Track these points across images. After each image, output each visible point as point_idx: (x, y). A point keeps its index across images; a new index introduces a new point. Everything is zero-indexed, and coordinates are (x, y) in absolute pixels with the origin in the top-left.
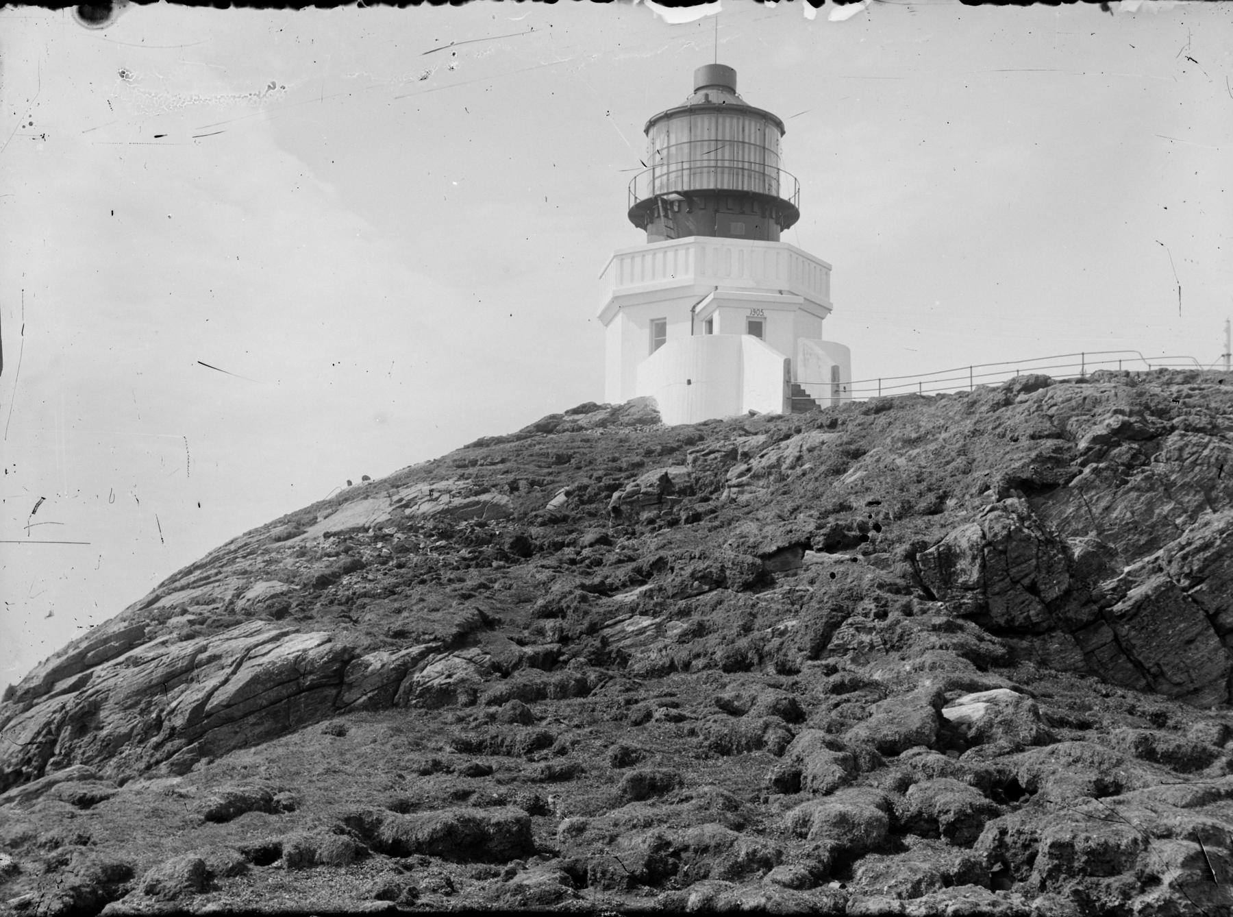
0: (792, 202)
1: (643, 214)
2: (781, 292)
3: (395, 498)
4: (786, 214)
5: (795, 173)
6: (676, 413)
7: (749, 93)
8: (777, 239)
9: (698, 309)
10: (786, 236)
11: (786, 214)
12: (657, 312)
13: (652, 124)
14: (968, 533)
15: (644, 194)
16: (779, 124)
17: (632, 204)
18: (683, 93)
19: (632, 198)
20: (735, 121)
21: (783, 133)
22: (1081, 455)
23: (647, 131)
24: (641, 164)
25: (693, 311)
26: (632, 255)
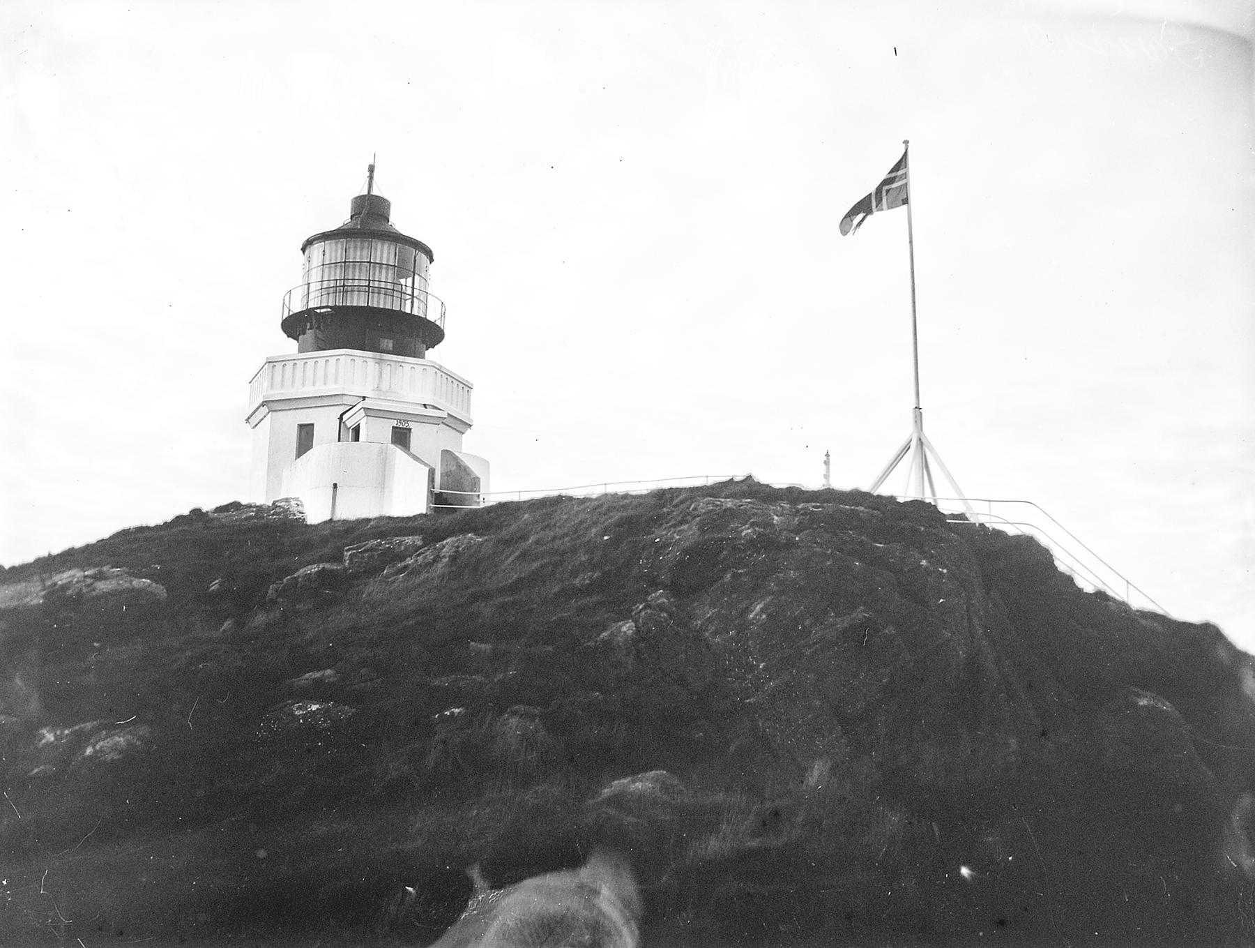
0: (438, 323)
1: (294, 325)
2: (425, 406)
3: (48, 583)
4: (431, 334)
5: (437, 294)
6: (315, 514)
7: (400, 221)
8: (423, 357)
9: (345, 417)
10: (430, 354)
11: (431, 334)
12: (305, 417)
13: (309, 243)
14: (624, 629)
15: (297, 307)
16: (429, 254)
17: (286, 315)
18: (341, 217)
19: (286, 310)
20: (386, 246)
21: (431, 260)
22: (501, 591)
23: (303, 250)
24: (301, 283)
25: (341, 418)
26: (283, 361)
